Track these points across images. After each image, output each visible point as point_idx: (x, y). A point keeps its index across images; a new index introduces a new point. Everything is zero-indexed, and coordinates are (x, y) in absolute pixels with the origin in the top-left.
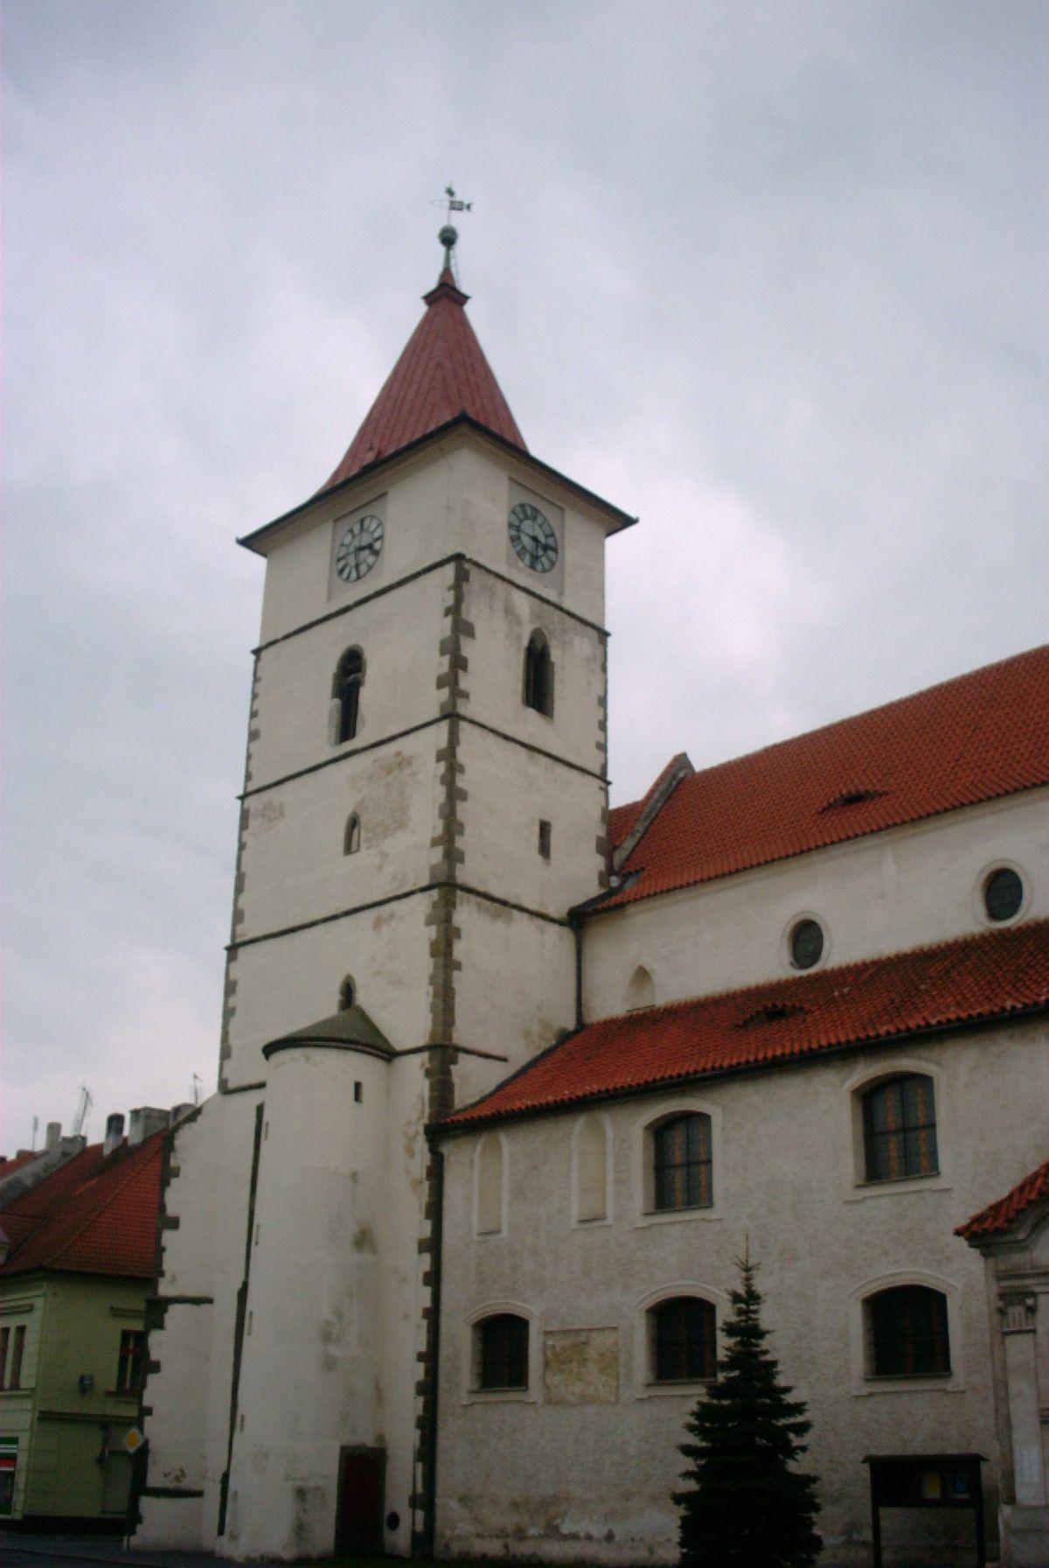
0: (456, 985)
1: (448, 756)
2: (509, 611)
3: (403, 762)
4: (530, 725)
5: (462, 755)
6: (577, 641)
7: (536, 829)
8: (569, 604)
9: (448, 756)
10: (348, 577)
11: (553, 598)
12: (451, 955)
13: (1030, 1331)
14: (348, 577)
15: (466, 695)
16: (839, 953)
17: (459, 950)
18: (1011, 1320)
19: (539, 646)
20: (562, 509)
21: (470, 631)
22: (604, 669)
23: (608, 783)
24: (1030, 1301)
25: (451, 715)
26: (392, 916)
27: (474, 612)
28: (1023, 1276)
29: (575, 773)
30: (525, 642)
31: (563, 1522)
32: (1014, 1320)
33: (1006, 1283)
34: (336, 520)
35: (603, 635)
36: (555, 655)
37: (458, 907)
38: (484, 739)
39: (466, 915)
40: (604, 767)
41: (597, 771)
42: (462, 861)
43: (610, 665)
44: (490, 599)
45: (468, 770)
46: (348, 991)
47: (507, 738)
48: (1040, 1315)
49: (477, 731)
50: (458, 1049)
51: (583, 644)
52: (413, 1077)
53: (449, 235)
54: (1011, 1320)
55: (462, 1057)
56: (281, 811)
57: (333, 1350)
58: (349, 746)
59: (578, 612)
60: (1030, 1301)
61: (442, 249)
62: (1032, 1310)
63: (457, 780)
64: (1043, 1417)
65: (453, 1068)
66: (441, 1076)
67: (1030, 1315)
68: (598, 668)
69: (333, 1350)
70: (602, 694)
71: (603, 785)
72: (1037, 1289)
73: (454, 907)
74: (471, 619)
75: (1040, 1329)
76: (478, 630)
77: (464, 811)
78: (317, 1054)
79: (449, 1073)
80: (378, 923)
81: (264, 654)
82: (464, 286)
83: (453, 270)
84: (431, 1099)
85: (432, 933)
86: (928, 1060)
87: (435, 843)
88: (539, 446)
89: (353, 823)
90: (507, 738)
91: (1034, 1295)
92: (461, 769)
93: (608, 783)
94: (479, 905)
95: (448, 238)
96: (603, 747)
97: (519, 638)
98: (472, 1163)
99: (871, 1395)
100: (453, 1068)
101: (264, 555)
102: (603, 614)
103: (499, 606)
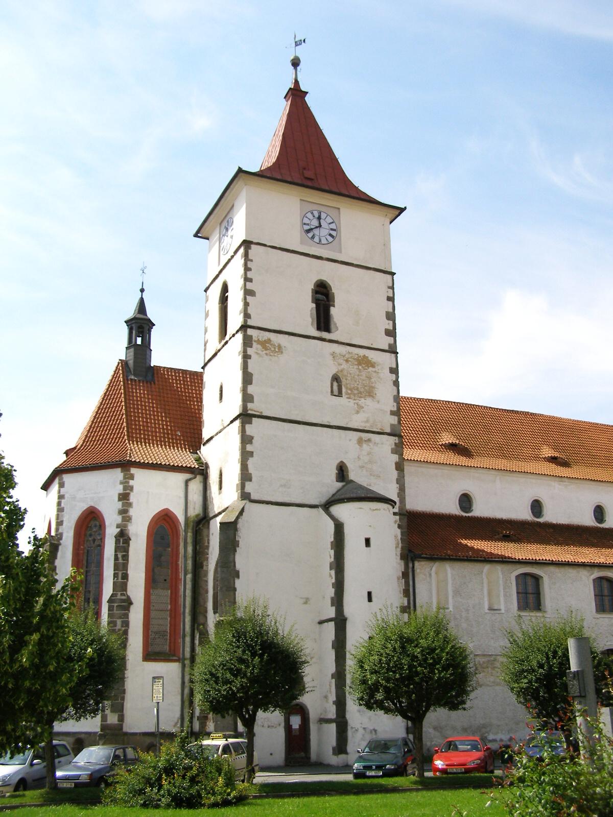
3: (369, 364)
10: (334, 230)
14: (334, 230)
16: (480, 510)
26: (369, 440)
31: (489, 735)
46: (342, 472)
53: (295, 61)
56: (280, 349)
58: (325, 335)
80: (360, 441)
85: (395, 458)
87: (392, 413)
89: (336, 379)
98: (430, 575)
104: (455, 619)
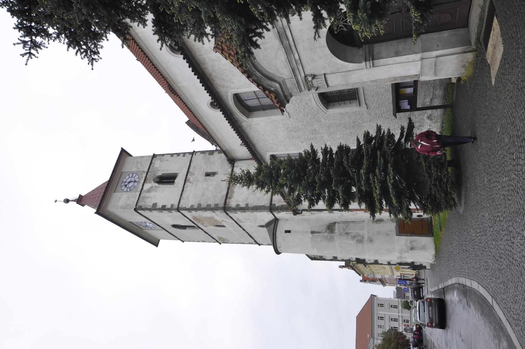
0: (253, 205)
1: (191, 209)
2: (149, 191)
4: (180, 181)
5: (188, 207)
6: (156, 166)
7: (208, 178)
8: (147, 171)
9: (191, 209)
11: (144, 175)
12: (244, 208)
13: (325, 77)
15: (172, 205)
17: (243, 205)
18: (320, 85)
19: (158, 179)
20: (122, 172)
21: (155, 205)
22: (163, 155)
23: (194, 151)
24: (310, 79)
25: (178, 210)
27: (149, 203)
28: (298, 82)
29: (192, 164)
30: (157, 185)
32: (320, 83)
33: (303, 88)
34: (142, 229)
35: (154, 156)
36: (160, 174)
37: (230, 206)
38: (184, 198)
39: (233, 203)
40: (190, 153)
41: (191, 155)
42: (218, 204)
43: (162, 153)
44: (146, 198)
45: (192, 204)
47: (183, 190)
48: (316, 73)
49: (181, 201)
50: (271, 204)
51: (157, 163)
52: (280, 215)
53: (65, 201)
54: (320, 85)
55: (273, 203)
59: (148, 166)
60: (310, 79)
61: (70, 202)
62: (314, 77)
63: (195, 208)
64: (370, 67)
65: (277, 205)
66: (279, 210)
67: (316, 77)
68: (163, 157)
69: (366, 238)
70: (170, 156)
71: (195, 153)
72: (303, 75)
73: (231, 207)
74: (152, 205)
75: (323, 72)
76: (154, 202)
77: (204, 205)
78: (278, 245)
79: (278, 207)
81: (183, 240)
82: (77, 197)
83: (74, 199)
84: (286, 212)
86: (227, 96)
88: (107, 178)
90: (183, 190)
91: (306, 76)
92: (192, 206)
93: (194, 151)
94: (230, 198)
95: (67, 201)
96: (184, 154)
97: (156, 187)
99: (366, 104)
100: (277, 205)
101: (159, 240)
102: (149, 156)
103: (148, 195)
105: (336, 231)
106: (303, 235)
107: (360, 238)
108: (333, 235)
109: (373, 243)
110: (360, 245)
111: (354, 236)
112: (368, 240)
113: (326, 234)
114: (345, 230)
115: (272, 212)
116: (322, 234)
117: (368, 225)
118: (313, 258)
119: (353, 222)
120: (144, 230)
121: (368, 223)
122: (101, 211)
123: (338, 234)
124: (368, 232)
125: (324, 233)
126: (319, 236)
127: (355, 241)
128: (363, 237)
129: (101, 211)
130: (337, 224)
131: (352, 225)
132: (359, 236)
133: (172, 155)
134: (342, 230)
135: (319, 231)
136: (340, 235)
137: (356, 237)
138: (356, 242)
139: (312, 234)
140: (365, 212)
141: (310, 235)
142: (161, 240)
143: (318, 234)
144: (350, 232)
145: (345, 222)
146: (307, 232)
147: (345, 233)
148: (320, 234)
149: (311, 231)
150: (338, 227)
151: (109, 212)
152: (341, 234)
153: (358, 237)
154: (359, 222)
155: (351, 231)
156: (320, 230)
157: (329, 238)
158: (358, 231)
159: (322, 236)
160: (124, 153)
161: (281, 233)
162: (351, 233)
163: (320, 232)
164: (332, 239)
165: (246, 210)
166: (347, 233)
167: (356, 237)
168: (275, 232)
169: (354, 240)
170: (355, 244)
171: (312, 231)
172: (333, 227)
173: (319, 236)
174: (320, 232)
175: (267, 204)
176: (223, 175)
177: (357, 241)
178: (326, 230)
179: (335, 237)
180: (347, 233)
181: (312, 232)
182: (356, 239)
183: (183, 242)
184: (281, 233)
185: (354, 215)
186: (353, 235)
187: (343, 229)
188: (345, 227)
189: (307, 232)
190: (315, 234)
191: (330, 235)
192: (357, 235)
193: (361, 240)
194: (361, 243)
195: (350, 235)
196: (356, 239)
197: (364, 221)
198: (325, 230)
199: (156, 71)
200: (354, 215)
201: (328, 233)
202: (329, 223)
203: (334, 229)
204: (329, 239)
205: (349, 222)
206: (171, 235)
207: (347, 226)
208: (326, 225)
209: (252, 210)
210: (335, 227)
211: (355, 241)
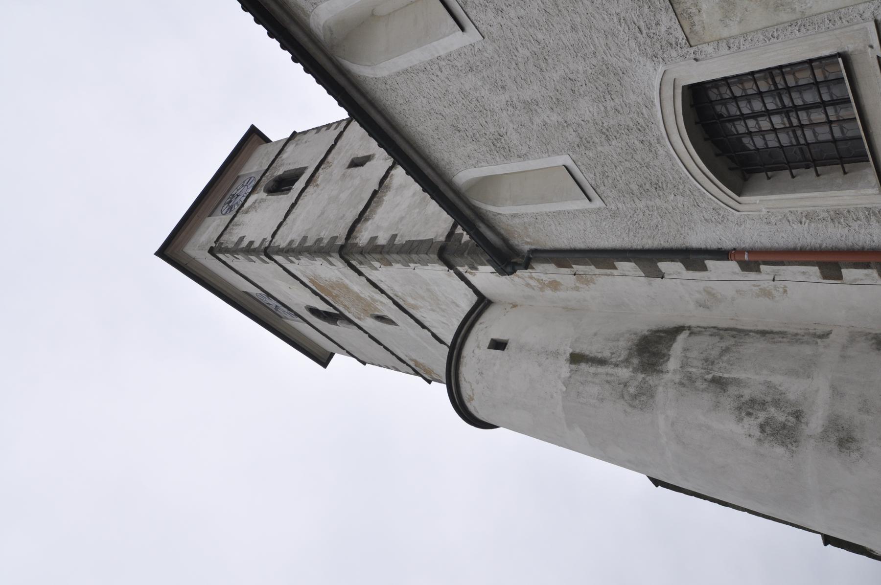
5: (283, 245)
17: (382, 240)
20: (238, 177)
34: (281, 317)
57: (815, 423)
69: (815, 423)
104: (585, 143)
105: (673, 364)
106: (540, 365)
107: (781, 418)
108: (652, 380)
109: (855, 455)
110: (780, 450)
111: (752, 401)
112: (825, 431)
113: (624, 373)
114: (713, 363)
115: (451, 266)
116: (609, 369)
117: (843, 357)
118: (657, 482)
119: (763, 333)
120: (284, 320)
121: (844, 347)
122: (168, 252)
123: (677, 378)
124: (837, 392)
125: (616, 365)
126: (595, 374)
127: (751, 425)
128: (798, 415)
129: (168, 252)
130: (682, 338)
131: (753, 347)
132: (776, 403)
133: (318, 129)
134: (699, 364)
135: (599, 356)
136: (682, 384)
137: (763, 404)
138: (757, 432)
139: (573, 366)
140: (825, 277)
141: (565, 369)
142: (336, 354)
143: (593, 370)
144: (732, 376)
145: (726, 330)
146: (556, 354)
147: (710, 377)
148: (601, 369)
149: (571, 351)
150: (686, 350)
151: (189, 256)
152: (688, 381)
153: (773, 410)
154: (796, 338)
155: (742, 376)
156: (606, 354)
157: (632, 390)
158: (776, 379)
159: (609, 379)
160: (256, 137)
161: (478, 347)
162: (737, 382)
163: (602, 362)
164: (644, 398)
165: (393, 253)
166: (720, 383)
167: (763, 404)
168: (459, 340)
169: (747, 420)
170: (751, 443)
171: (577, 351)
172: (661, 347)
173: (595, 374)
174: (602, 362)
175: (441, 235)
176: (382, 161)
177: (762, 427)
178: (630, 356)
179: (660, 389)
180: (720, 383)
181: (576, 358)
182: (762, 416)
183: (364, 363)
184: (478, 347)
185: (766, 293)
186: (747, 393)
187: (706, 360)
188: (715, 353)
189: (556, 354)
190: (583, 366)
191: (641, 376)
192: (768, 399)
193: (784, 426)
194: (783, 444)
195: (733, 390)
196: (762, 416)
197: (825, 335)
198: (624, 355)
199: (507, 99)
200: (766, 293)
201: (635, 370)
202: (654, 328)
203: (664, 355)
204: (635, 397)
205: (745, 333)
206: (324, 337)
207: (726, 350)
208: (635, 334)
209: (397, 253)
210: (669, 347)
211: (751, 425)
